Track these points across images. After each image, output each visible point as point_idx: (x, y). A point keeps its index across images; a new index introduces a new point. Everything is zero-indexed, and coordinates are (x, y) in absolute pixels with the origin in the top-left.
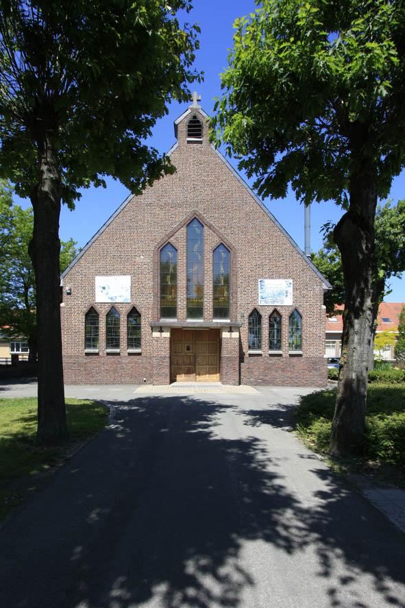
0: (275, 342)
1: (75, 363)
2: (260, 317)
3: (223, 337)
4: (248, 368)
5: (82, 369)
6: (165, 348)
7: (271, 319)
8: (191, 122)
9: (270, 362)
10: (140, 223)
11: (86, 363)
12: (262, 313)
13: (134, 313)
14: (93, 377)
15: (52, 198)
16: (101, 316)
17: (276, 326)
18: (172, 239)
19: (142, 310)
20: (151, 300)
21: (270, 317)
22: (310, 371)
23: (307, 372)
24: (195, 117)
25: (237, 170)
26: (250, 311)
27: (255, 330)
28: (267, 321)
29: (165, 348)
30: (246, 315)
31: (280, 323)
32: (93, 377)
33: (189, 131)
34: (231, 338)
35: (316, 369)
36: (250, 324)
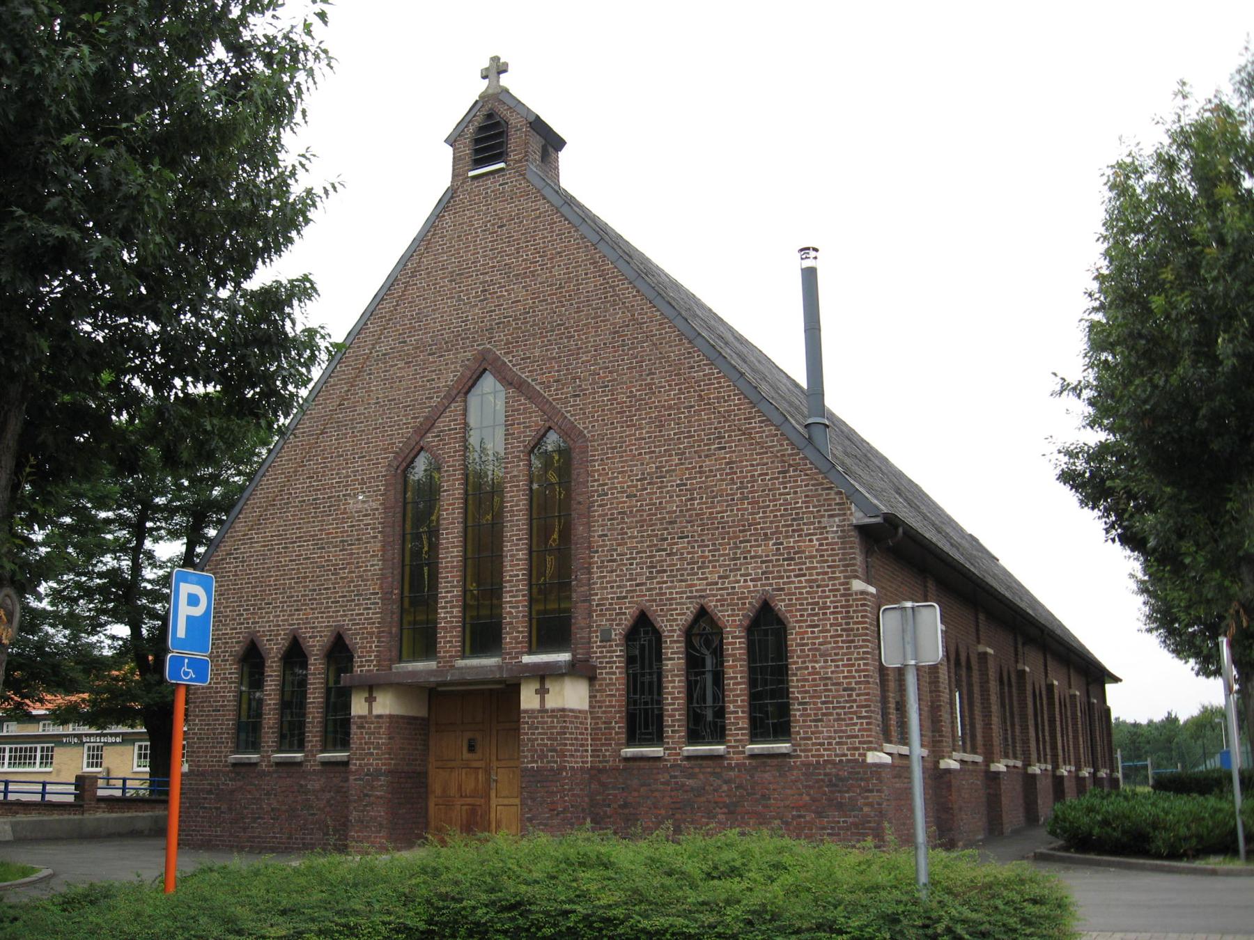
0: (709, 715)
1: (210, 792)
2: (657, 635)
3: (353, 713)
4: (625, 806)
5: (224, 807)
6: (378, 747)
7: (696, 641)
8: (481, 129)
9: (689, 782)
10: (360, 409)
11: (232, 792)
12: (663, 624)
13: (339, 652)
14: (245, 829)
15: (199, 390)
16: (268, 663)
17: (709, 663)
18: (429, 437)
19: (356, 641)
20: (374, 613)
21: (689, 633)
22: (820, 814)
23: (810, 816)
24: (490, 116)
25: (702, 601)
26: (627, 621)
27: (647, 679)
28: (680, 647)
29: (378, 747)
30: (617, 633)
31: (719, 653)
32: (245, 829)
33: (477, 151)
34: (543, 710)
35: (840, 806)
36: (630, 660)
